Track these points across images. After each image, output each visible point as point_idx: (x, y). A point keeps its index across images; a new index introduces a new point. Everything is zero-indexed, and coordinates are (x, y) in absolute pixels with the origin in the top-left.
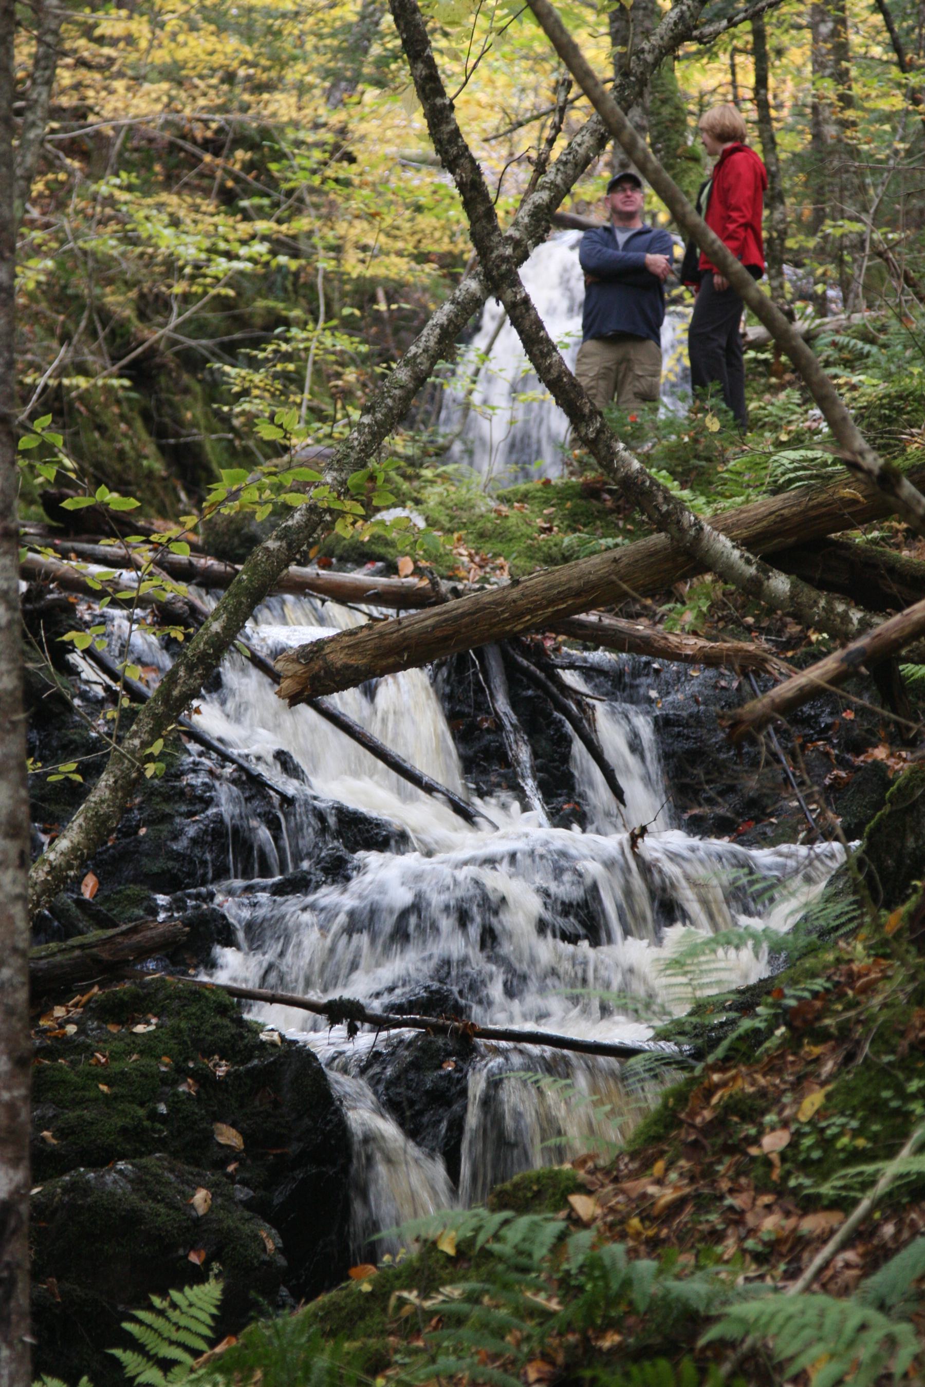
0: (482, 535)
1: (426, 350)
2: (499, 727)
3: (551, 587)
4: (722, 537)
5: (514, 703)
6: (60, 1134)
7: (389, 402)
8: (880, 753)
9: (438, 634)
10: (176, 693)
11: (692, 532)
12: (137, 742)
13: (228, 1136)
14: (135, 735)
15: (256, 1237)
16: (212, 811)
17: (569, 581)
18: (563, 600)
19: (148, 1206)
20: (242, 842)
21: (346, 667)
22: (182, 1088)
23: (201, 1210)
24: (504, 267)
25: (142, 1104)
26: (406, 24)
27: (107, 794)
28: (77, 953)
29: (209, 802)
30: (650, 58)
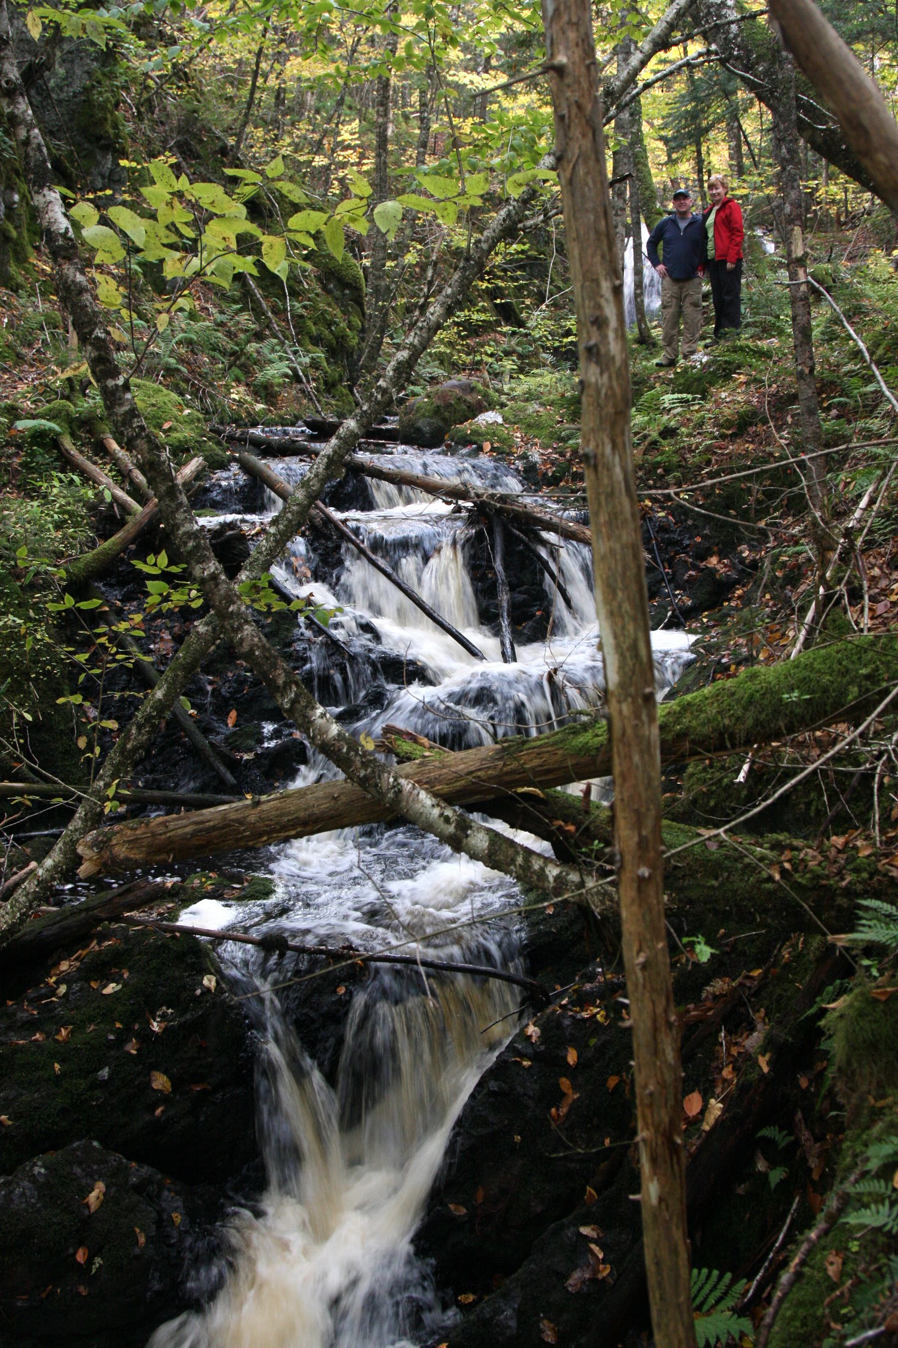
0: (529, 426)
1: (316, 476)
4: (423, 795)
5: (506, 567)
7: (289, 515)
10: (129, 746)
11: (391, 795)
12: (102, 783)
14: (101, 778)
16: (308, 666)
17: (297, 811)
20: (325, 681)
21: (127, 859)
24: (191, 544)
26: (73, 305)
28: (83, 915)
29: (306, 660)
30: (485, 246)
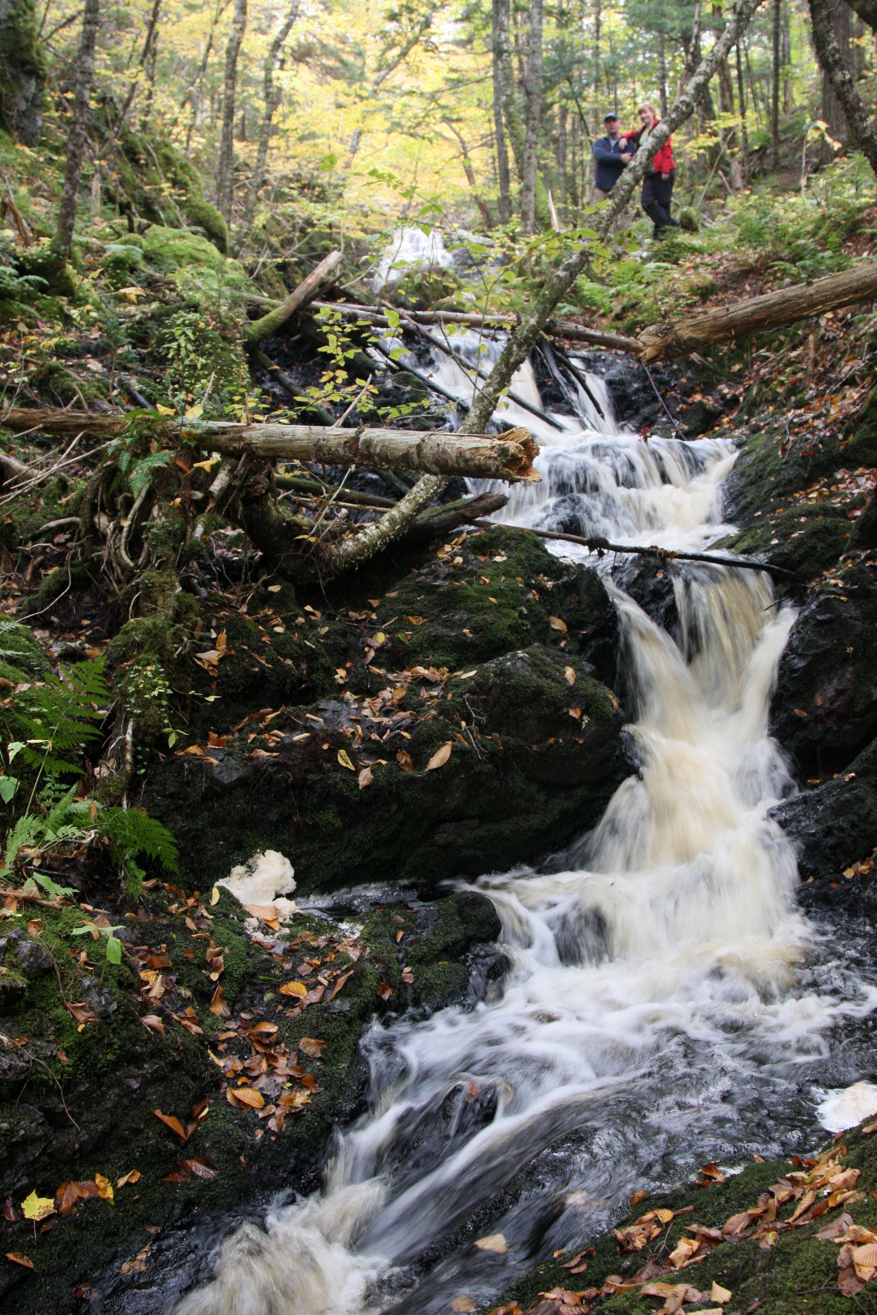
2: (558, 384)
3: (838, 286)
6: (474, 630)
8: (698, 397)
9: (756, 317)
13: (558, 624)
15: (606, 699)
18: (846, 295)
19: (544, 682)
21: (691, 339)
22: (530, 596)
23: (571, 681)
25: (514, 608)
27: (476, 421)
